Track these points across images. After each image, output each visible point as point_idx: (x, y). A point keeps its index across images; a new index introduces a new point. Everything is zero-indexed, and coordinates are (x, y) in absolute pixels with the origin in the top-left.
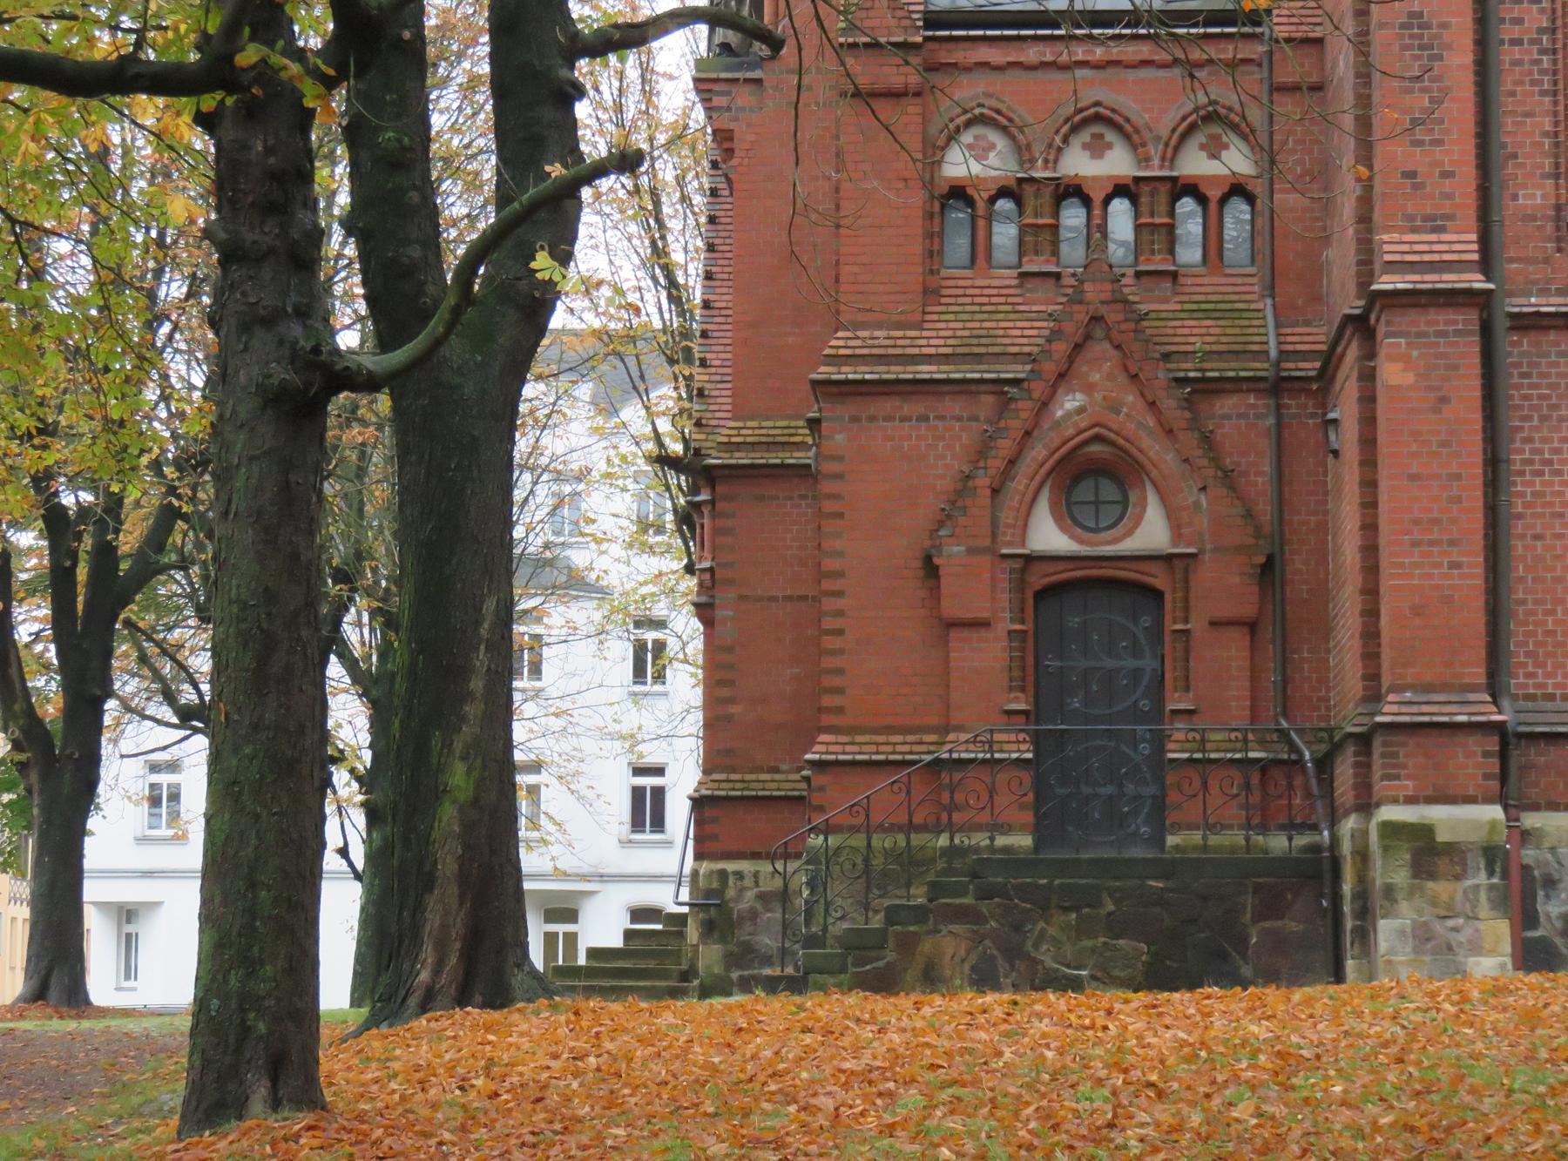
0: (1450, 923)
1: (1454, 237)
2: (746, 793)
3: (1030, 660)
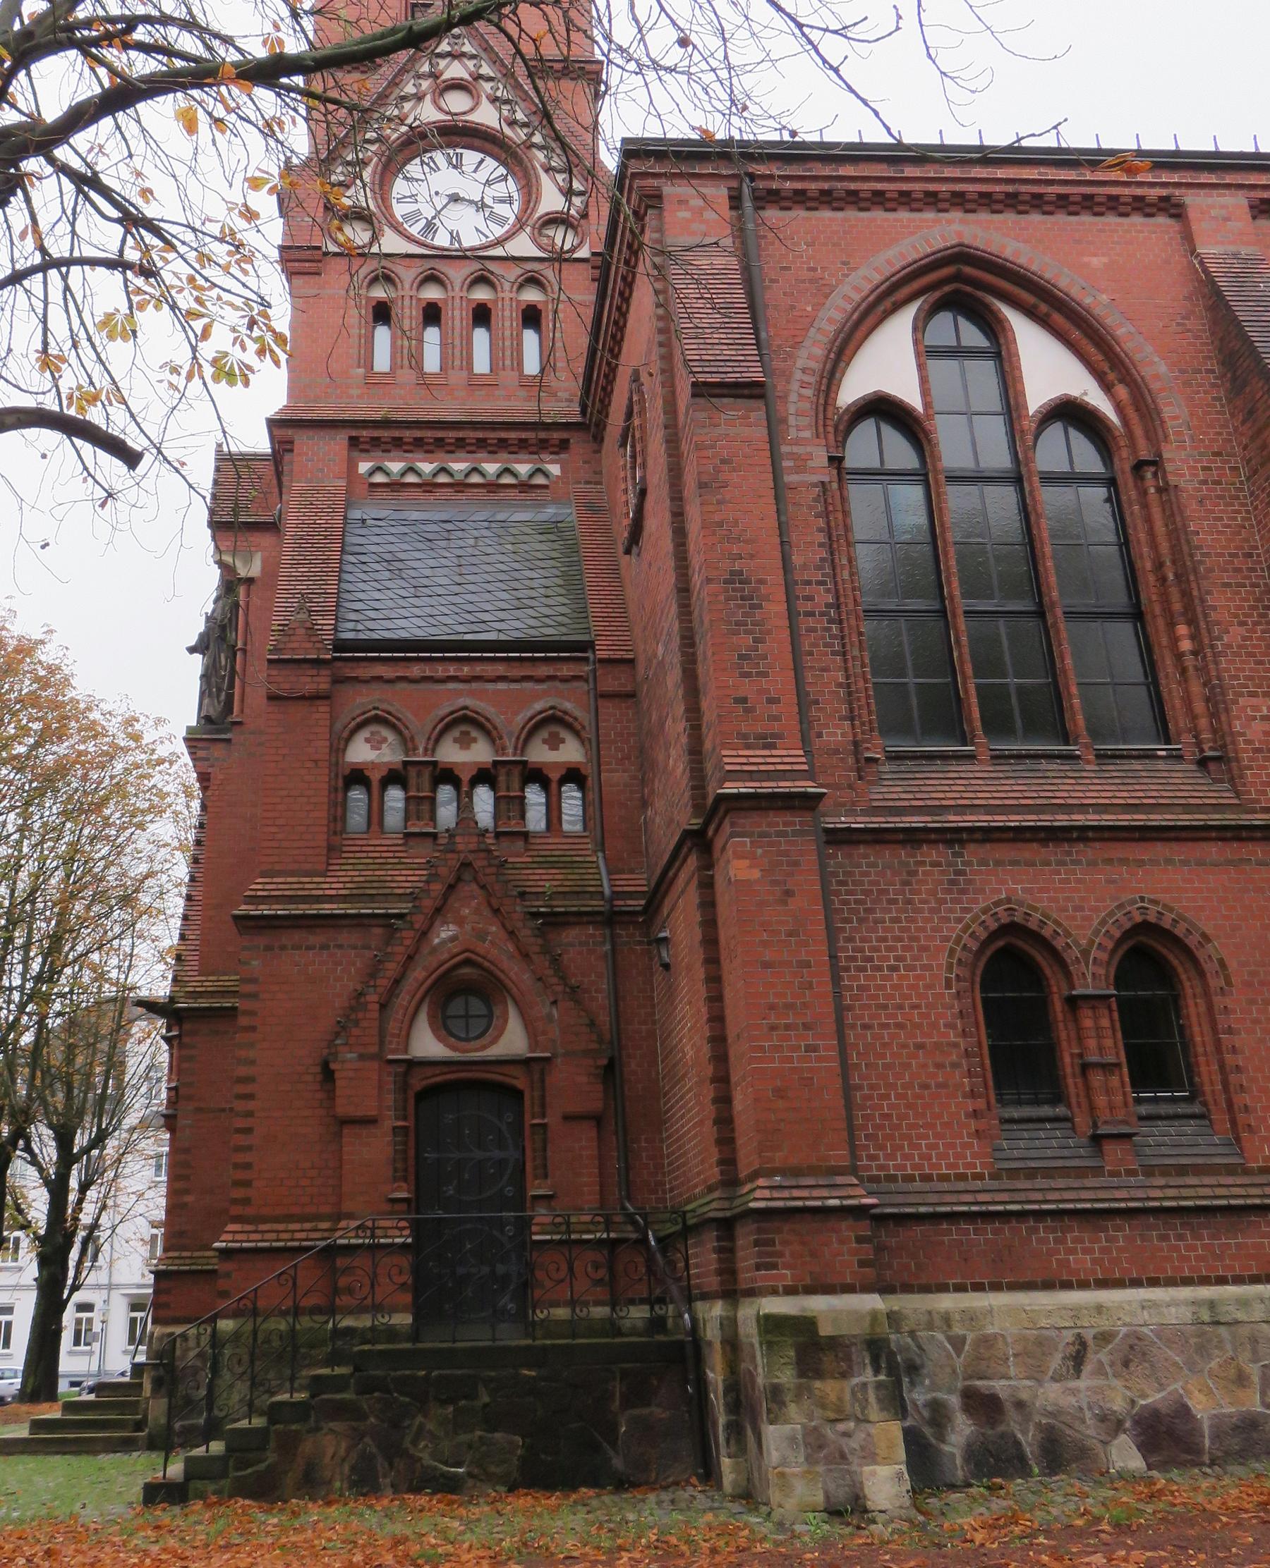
0: (841, 1427)
1: (785, 753)
2: (194, 1267)
3: (412, 1153)
